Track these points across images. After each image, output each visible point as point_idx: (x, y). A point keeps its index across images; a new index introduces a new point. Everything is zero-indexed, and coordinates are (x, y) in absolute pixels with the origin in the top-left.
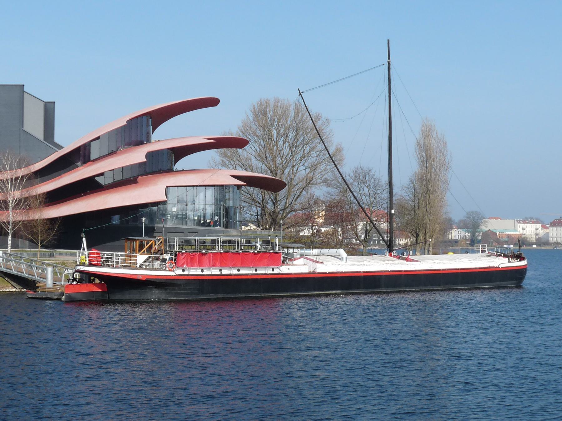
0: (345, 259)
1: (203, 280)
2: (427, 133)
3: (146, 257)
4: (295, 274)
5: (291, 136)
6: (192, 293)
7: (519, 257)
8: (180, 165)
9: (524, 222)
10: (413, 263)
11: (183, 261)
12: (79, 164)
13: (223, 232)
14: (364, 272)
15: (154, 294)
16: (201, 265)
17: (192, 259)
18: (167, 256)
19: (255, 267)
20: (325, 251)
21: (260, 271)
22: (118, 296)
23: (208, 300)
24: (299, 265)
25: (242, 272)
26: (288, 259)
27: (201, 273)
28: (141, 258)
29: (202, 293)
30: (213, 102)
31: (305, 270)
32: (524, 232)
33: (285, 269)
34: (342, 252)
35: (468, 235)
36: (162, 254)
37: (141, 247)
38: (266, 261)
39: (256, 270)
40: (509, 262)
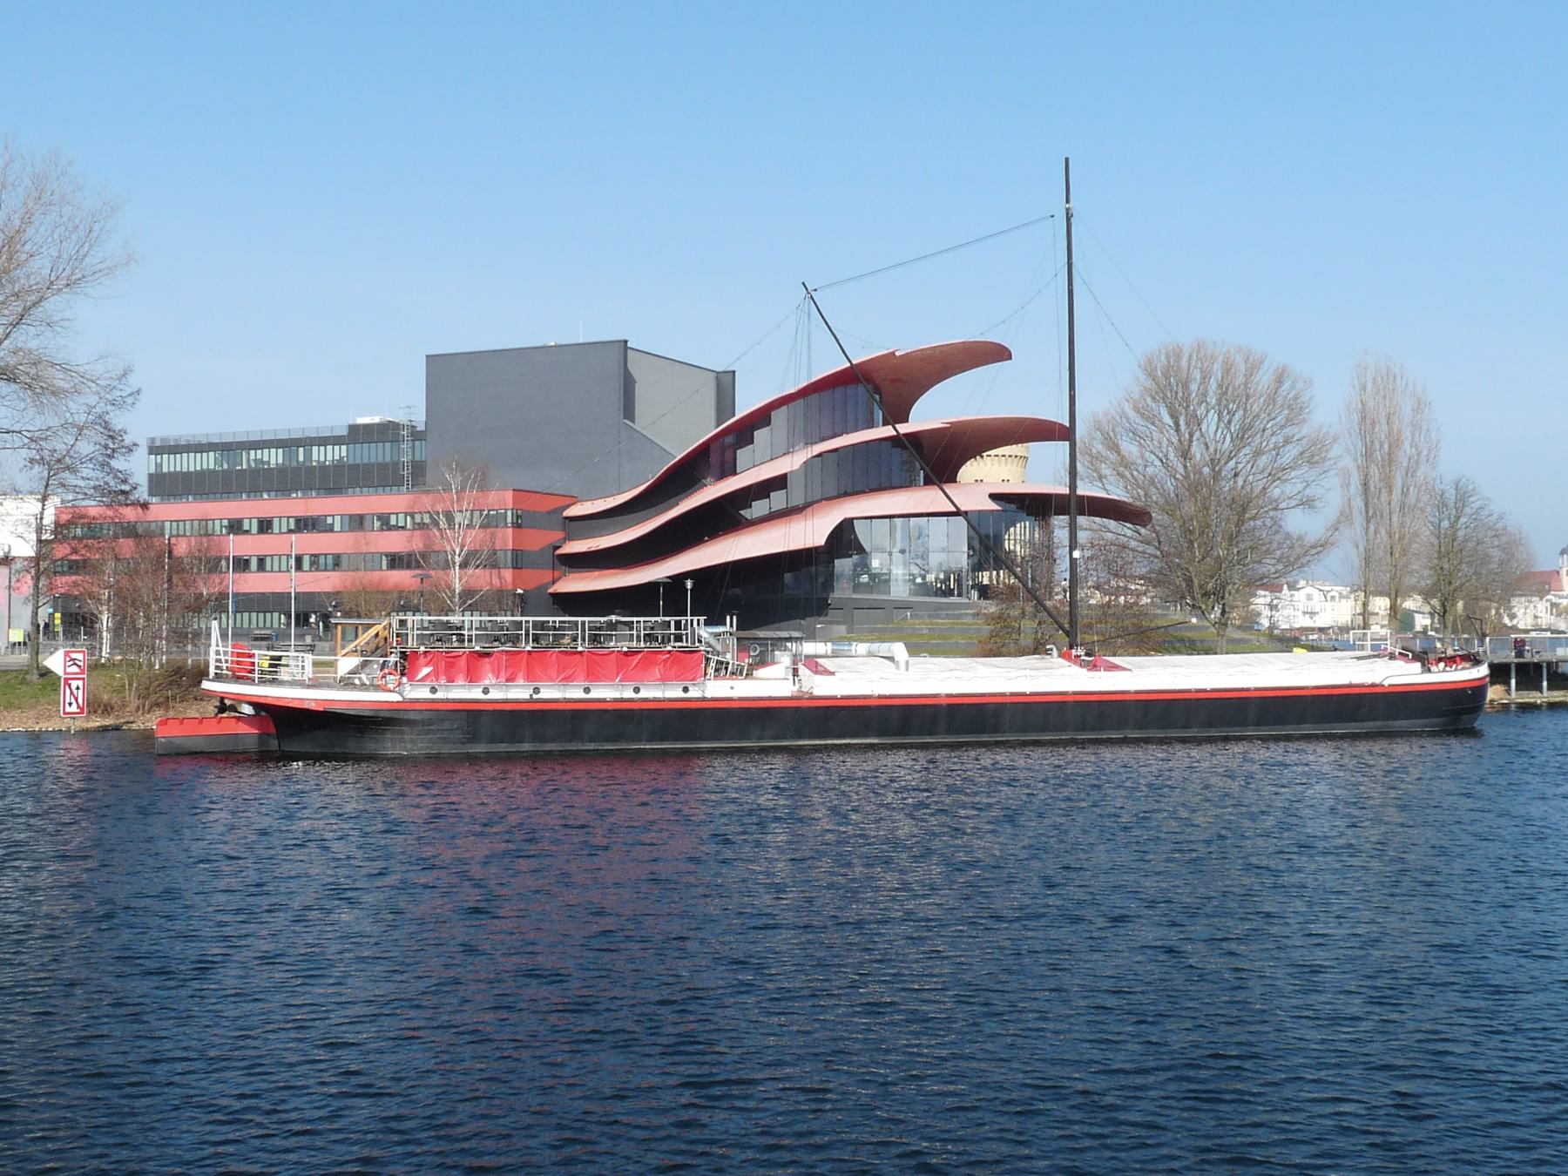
0: (902, 665)
6: (446, 740)
7: (1475, 661)
16: (472, 677)
19: (634, 684)
20: (875, 646)
23: (492, 758)
27: (482, 696)
29: (473, 738)
33: (717, 689)
34: (899, 650)
35: (1048, 603)
39: (637, 690)
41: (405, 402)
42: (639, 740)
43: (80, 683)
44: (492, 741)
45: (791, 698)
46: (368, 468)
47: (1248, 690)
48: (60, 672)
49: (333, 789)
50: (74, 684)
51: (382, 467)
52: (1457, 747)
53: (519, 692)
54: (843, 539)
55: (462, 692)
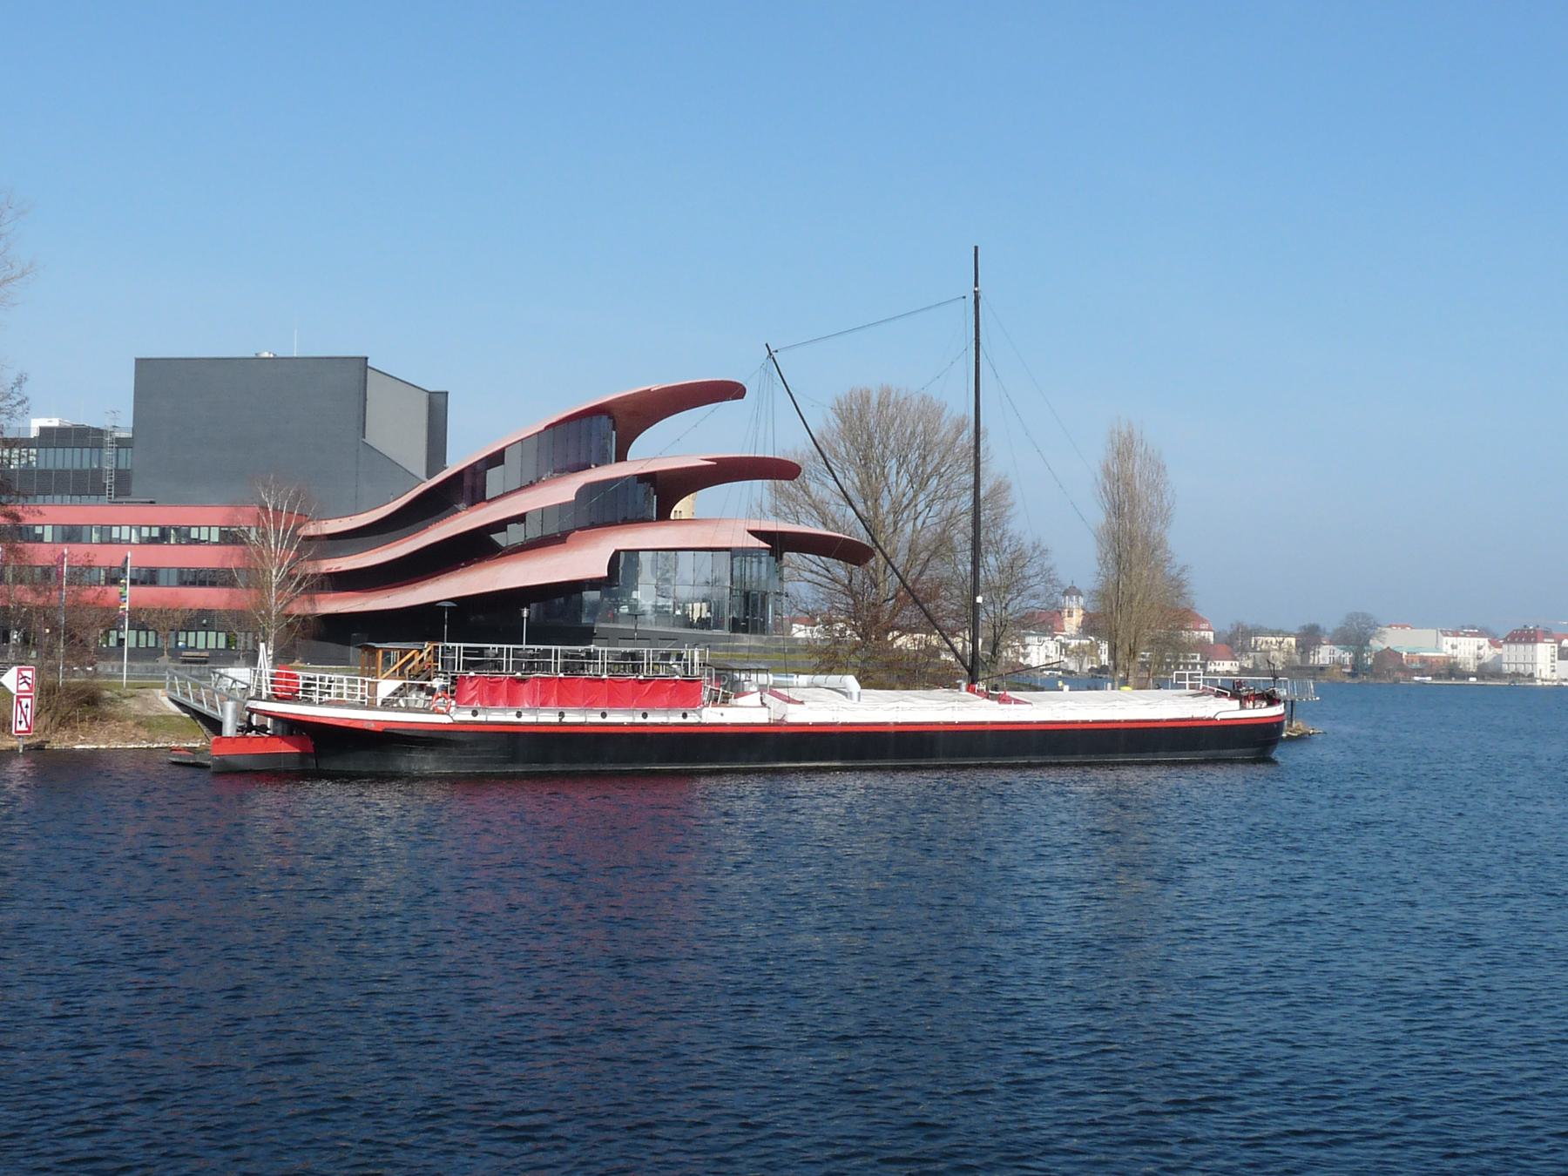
0: (855, 696)
1: (517, 734)
2: (1124, 450)
3: (398, 683)
4: (733, 725)
5: (914, 457)
7: (1272, 700)
8: (683, 507)
9: (1456, 634)
10: (1013, 706)
11: (473, 694)
12: (461, 506)
13: (729, 639)
14: (896, 724)
15: (427, 763)
16: (512, 701)
17: (493, 690)
18: (437, 683)
19: (644, 710)
20: (820, 679)
21: (652, 718)
22: (336, 765)
23: (528, 776)
24: (747, 711)
25: (610, 719)
26: (729, 690)
27: (515, 719)
28: (386, 687)
29: (513, 760)
30: (729, 391)
31: (760, 716)
32: (1455, 652)
33: (711, 715)
34: (851, 682)
35: (1347, 657)
36: (429, 679)
37: (387, 662)
38: (665, 698)
39: (645, 715)
40: (1243, 707)
41: (111, 407)
42: (649, 761)
43: (28, 701)
44: (529, 761)
45: (769, 725)
46: (62, 475)
47: (886, 724)
48: (13, 690)
49: (378, 809)
50: (25, 701)
51: (80, 474)
52: (1263, 769)
53: (549, 717)
54: (622, 566)
55: (502, 715)
